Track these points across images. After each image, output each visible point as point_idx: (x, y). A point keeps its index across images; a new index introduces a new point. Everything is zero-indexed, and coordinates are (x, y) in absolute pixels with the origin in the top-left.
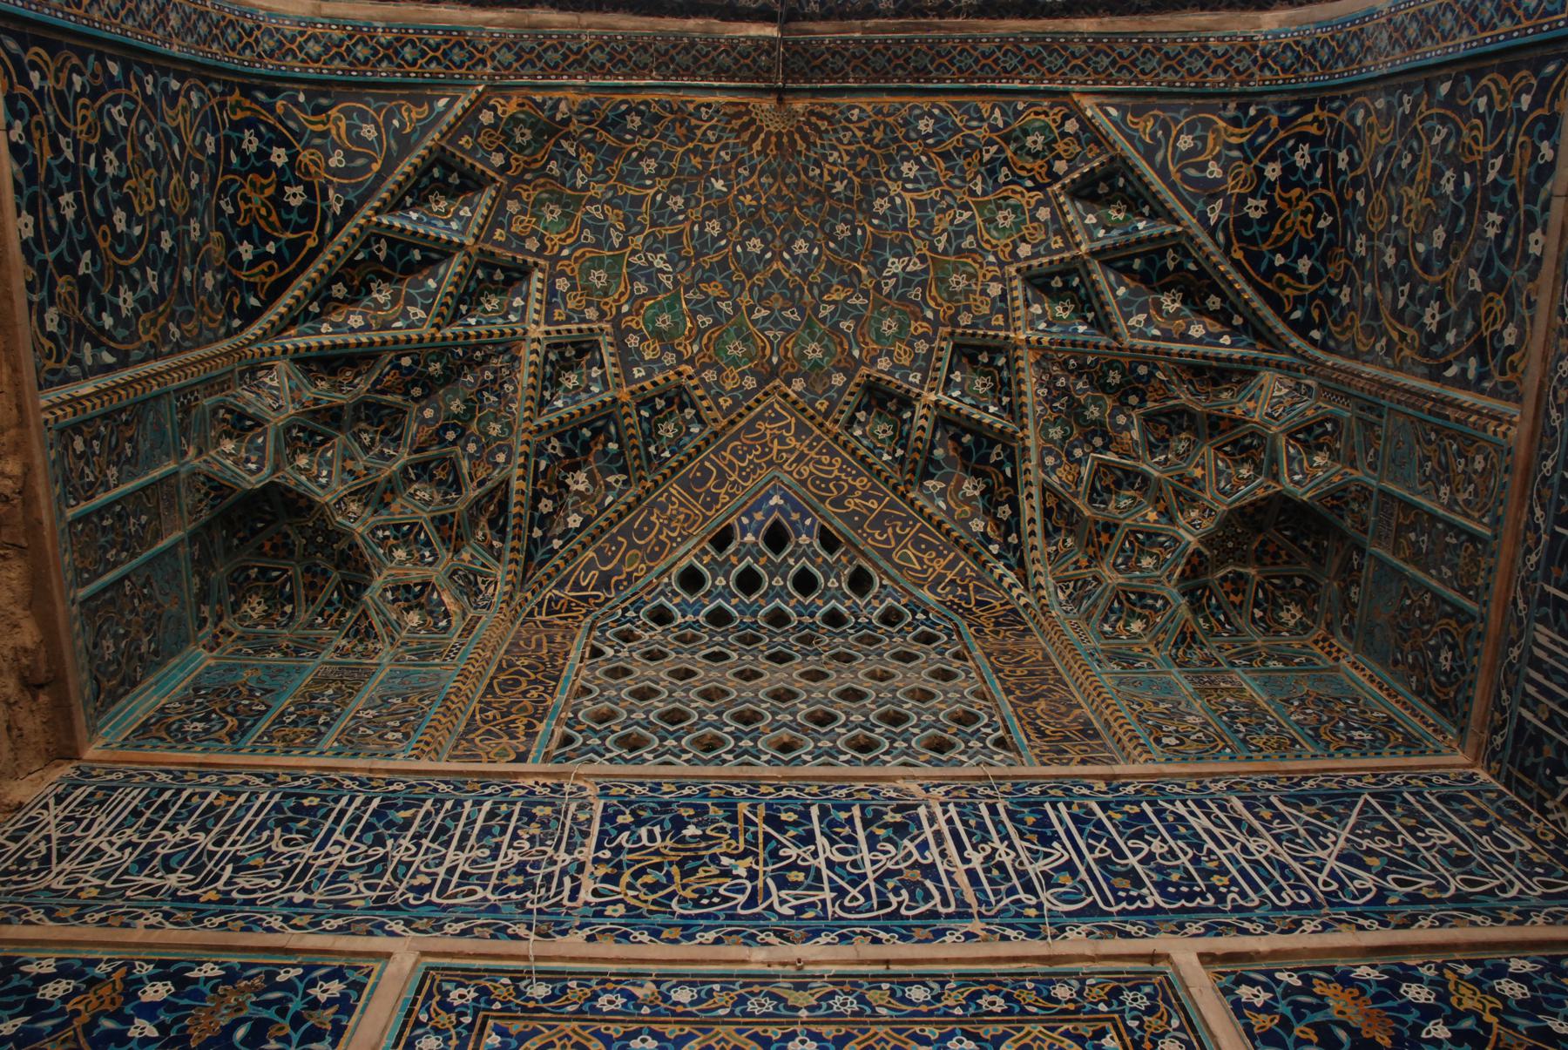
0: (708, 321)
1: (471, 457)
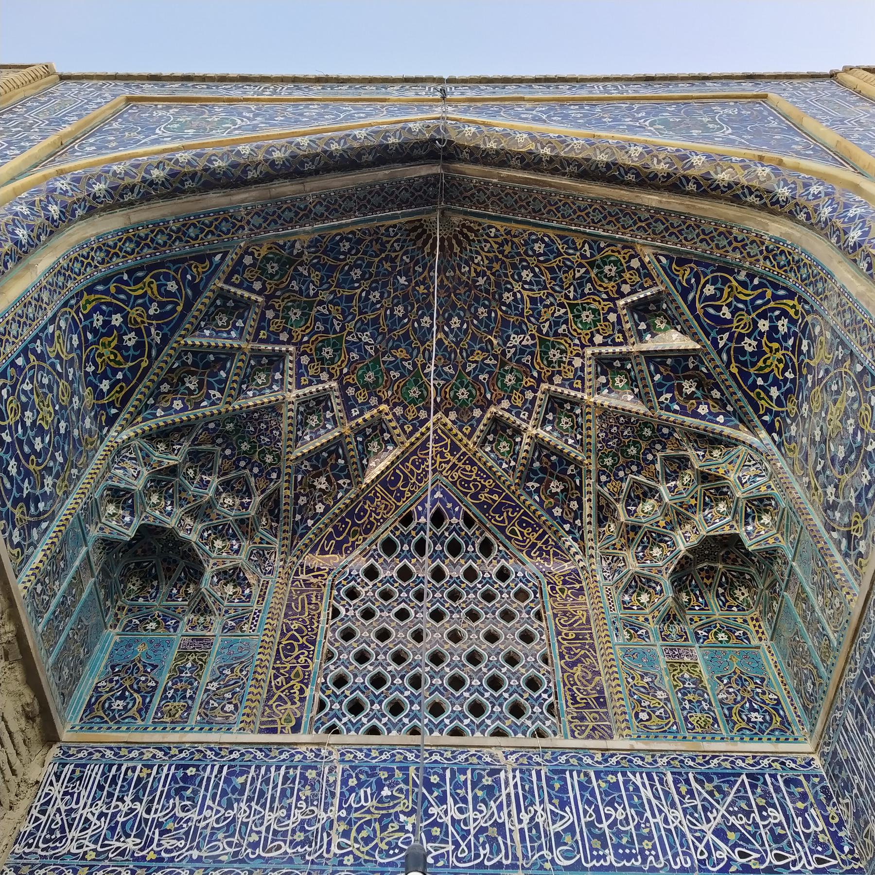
0: (397, 375)
1: (256, 476)
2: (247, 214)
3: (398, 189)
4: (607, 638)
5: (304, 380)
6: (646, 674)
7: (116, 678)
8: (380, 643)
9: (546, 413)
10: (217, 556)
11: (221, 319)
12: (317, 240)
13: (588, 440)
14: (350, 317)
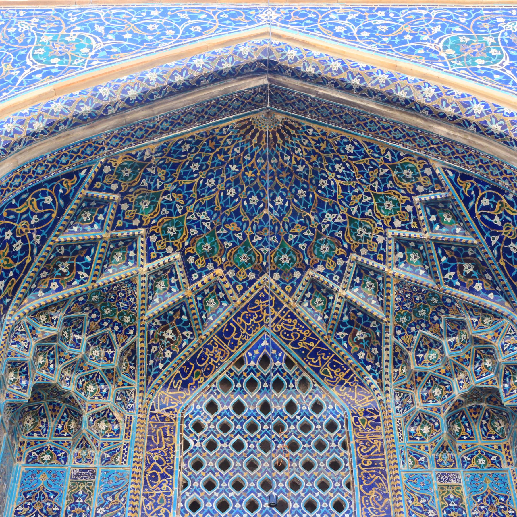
1: (116, 333)
2: (107, 139)
3: (230, 100)
4: (396, 466)
5: (153, 255)
6: (422, 496)
7: (29, 504)
8: (222, 472)
9: (354, 277)
10: (91, 400)
11: (86, 216)
12: (163, 147)
13: (388, 303)
14: (190, 201)
